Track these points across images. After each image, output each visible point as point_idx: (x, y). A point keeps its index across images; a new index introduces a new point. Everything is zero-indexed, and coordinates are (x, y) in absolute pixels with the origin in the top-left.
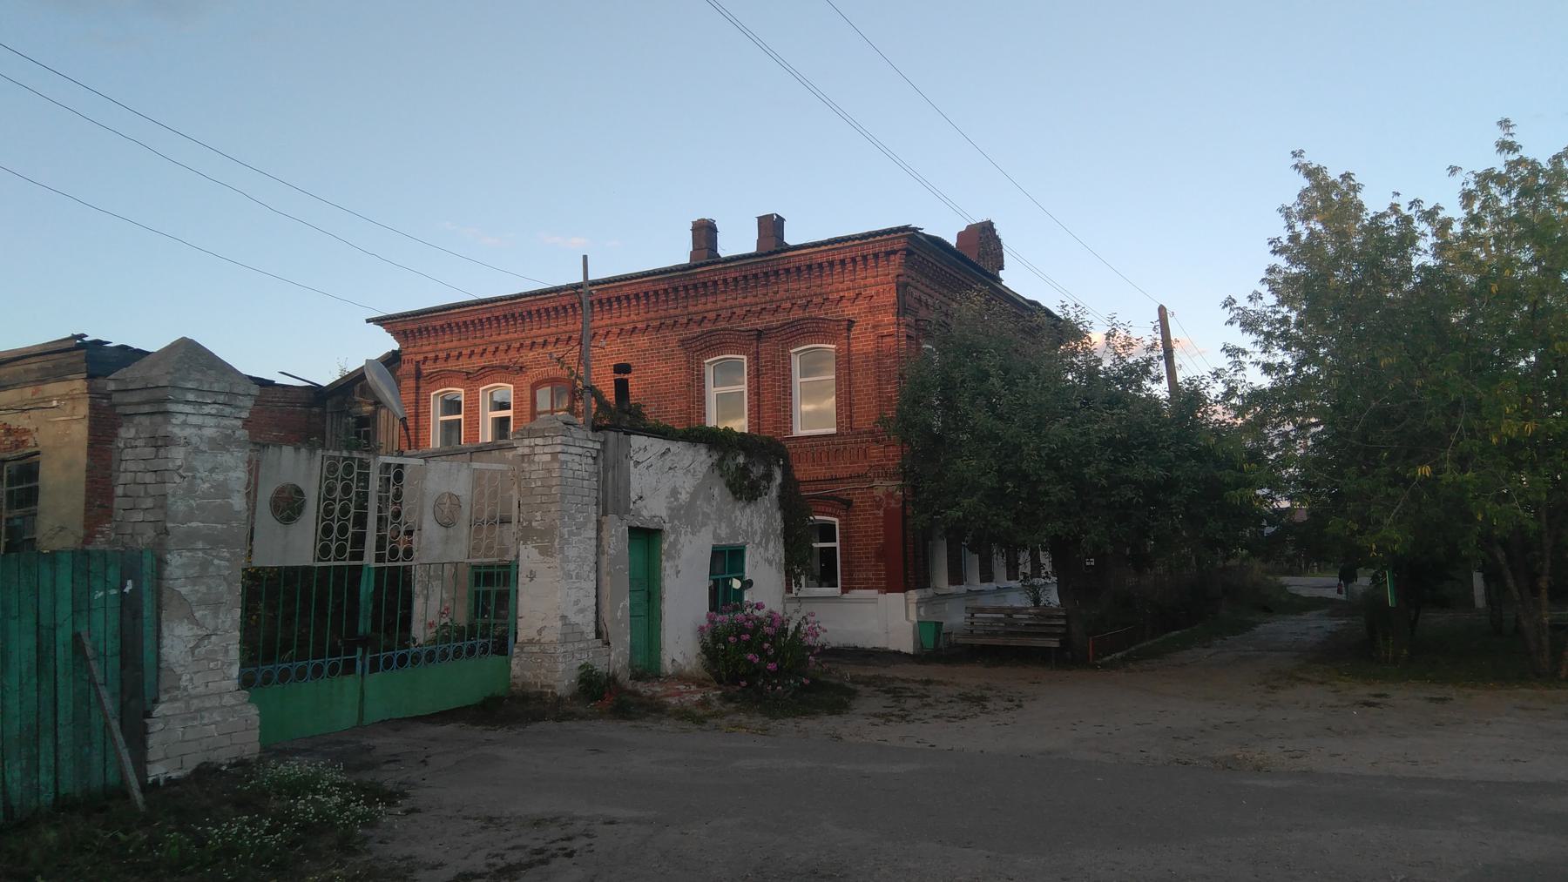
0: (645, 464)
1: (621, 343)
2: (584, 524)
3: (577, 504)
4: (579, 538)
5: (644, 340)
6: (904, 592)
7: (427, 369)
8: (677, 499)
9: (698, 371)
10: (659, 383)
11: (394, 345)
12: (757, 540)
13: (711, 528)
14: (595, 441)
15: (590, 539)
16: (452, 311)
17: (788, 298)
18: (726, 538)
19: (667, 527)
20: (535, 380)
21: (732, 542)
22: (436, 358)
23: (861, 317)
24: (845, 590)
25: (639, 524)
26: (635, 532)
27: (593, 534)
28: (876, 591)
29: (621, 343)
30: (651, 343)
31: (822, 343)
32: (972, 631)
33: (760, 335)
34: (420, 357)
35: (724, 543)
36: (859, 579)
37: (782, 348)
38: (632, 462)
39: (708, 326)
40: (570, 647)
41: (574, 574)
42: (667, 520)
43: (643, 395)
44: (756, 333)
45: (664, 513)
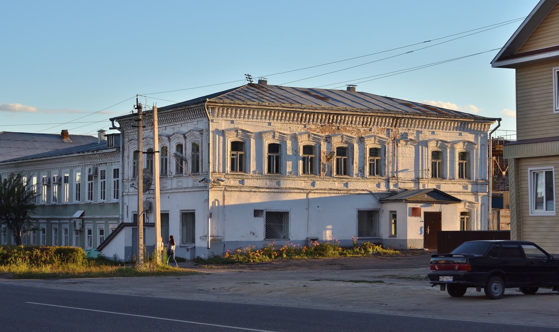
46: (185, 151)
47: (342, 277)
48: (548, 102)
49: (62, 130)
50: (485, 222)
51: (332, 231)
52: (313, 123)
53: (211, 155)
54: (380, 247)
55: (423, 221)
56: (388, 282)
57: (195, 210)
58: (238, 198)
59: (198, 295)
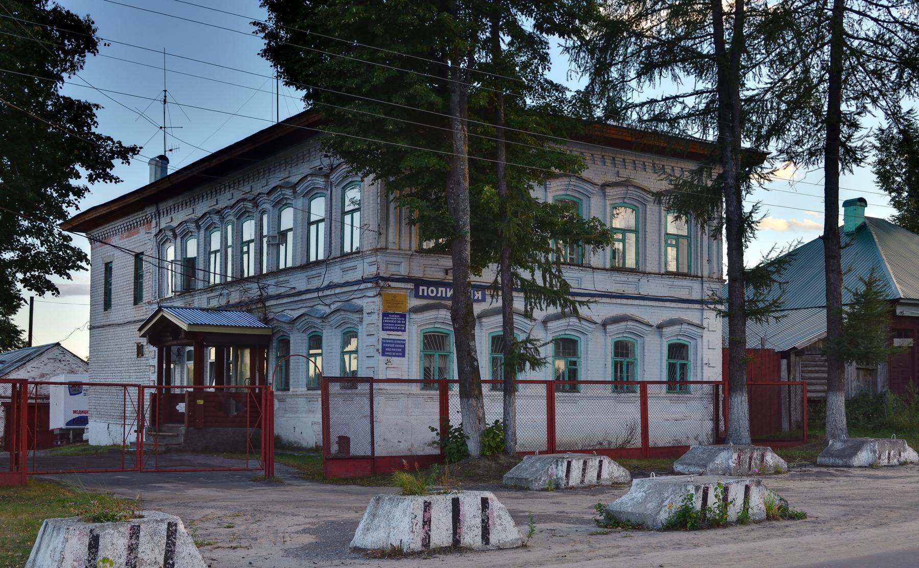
16: (304, 297)
46: (37, 553)
47: (305, 305)
48: (435, 339)
49: (339, 437)
50: (803, 406)
51: (317, 449)
52: (265, 314)
53: (464, 176)
54: (544, 307)
55: (420, 500)
56: (366, 190)
57: (87, 412)
58: (865, 107)
59: (671, 283)
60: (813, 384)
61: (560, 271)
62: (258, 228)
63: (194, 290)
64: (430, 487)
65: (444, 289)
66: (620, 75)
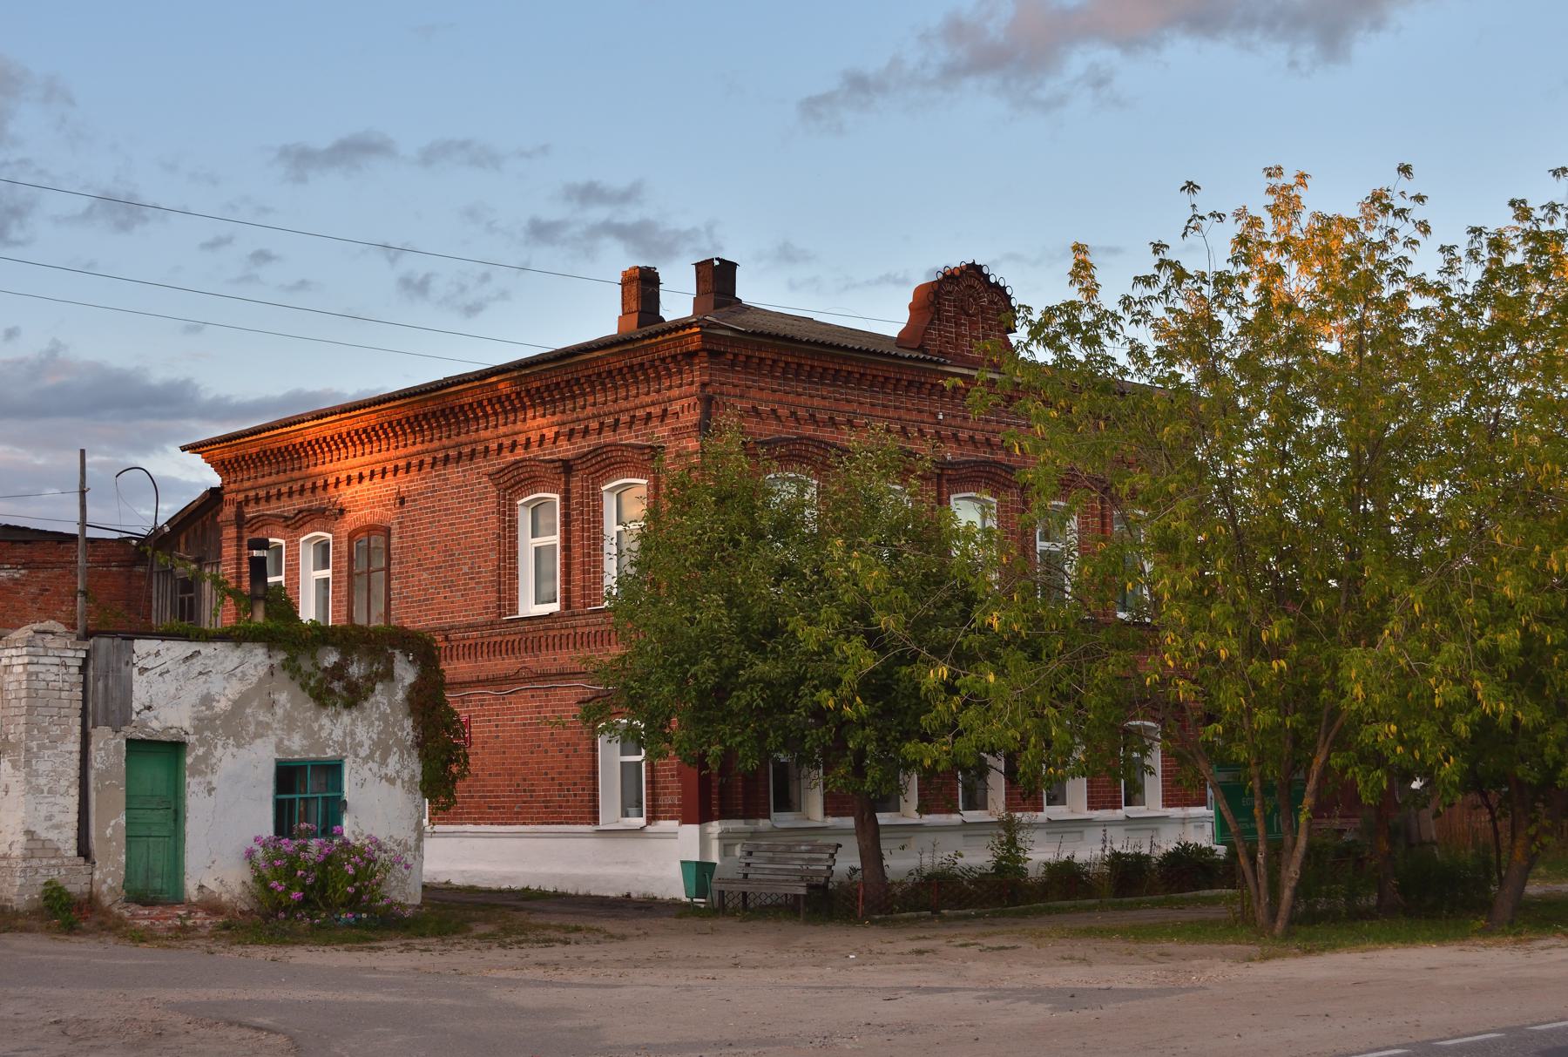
0: (158, 670)
1: (436, 476)
2: (63, 737)
3: (52, 716)
4: (55, 751)
5: (458, 472)
6: (700, 824)
7: (250, 512)
8: (210, 708)
9: (510, 516)
10: (472, 532)
11: (215, 480)
12: (363, 752)
13: (273, 739)
14: (76, 650)
15: (71, 753)
16: (263, 435)
17: (594, 416)
18: (298, 747)
19: (192, 739)
20: (353, 527)
21: (313, 755)
22: (302, 491)
23: (670, 442)
24: (652, 819)
25: (144, 736)
26: (137, 747)
27: (77, 747)
28: (677, 822)
29: (436, 476)
30: (465, 476)
31: (634, 477)
32: (746, 876)
33: (567, 467)
34: (241, 497)
35: (296, 757)
36: (665, 806)
37: (593, 484)
38: (135, 670)
39: (520, 453)
40: (35, 862)
41: (46, 789)
42: (191, 731)
43: (457, 550)
44: (560, 464)
45: (186, 725)
60: (795, 881)
61: (344, 737)
62: (624, 835)
63: (91, 892)
64: (896, 915)
65: (361, 619)
66: (1193, 424)
